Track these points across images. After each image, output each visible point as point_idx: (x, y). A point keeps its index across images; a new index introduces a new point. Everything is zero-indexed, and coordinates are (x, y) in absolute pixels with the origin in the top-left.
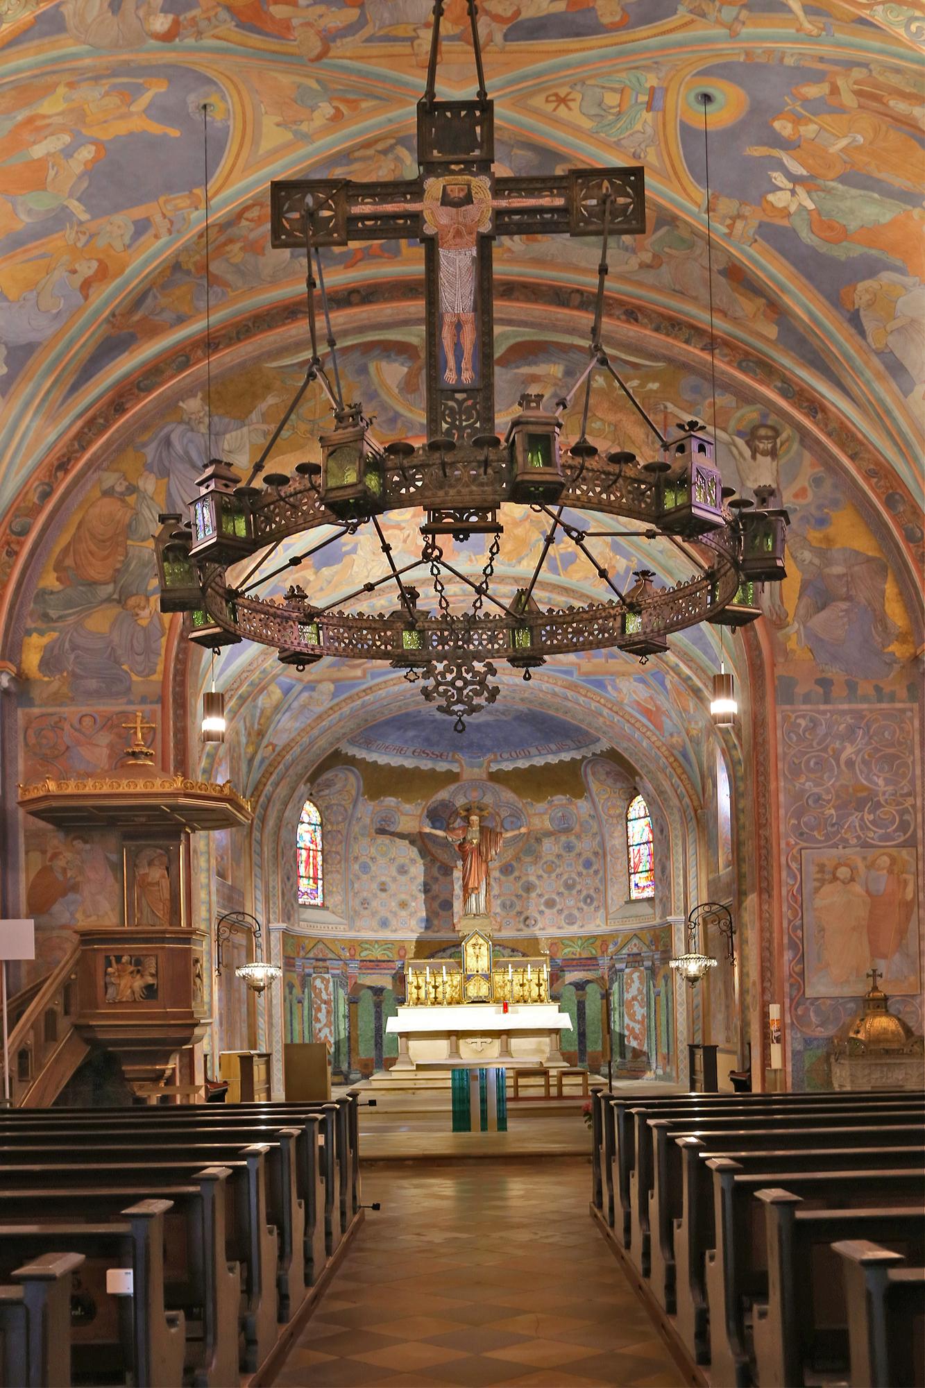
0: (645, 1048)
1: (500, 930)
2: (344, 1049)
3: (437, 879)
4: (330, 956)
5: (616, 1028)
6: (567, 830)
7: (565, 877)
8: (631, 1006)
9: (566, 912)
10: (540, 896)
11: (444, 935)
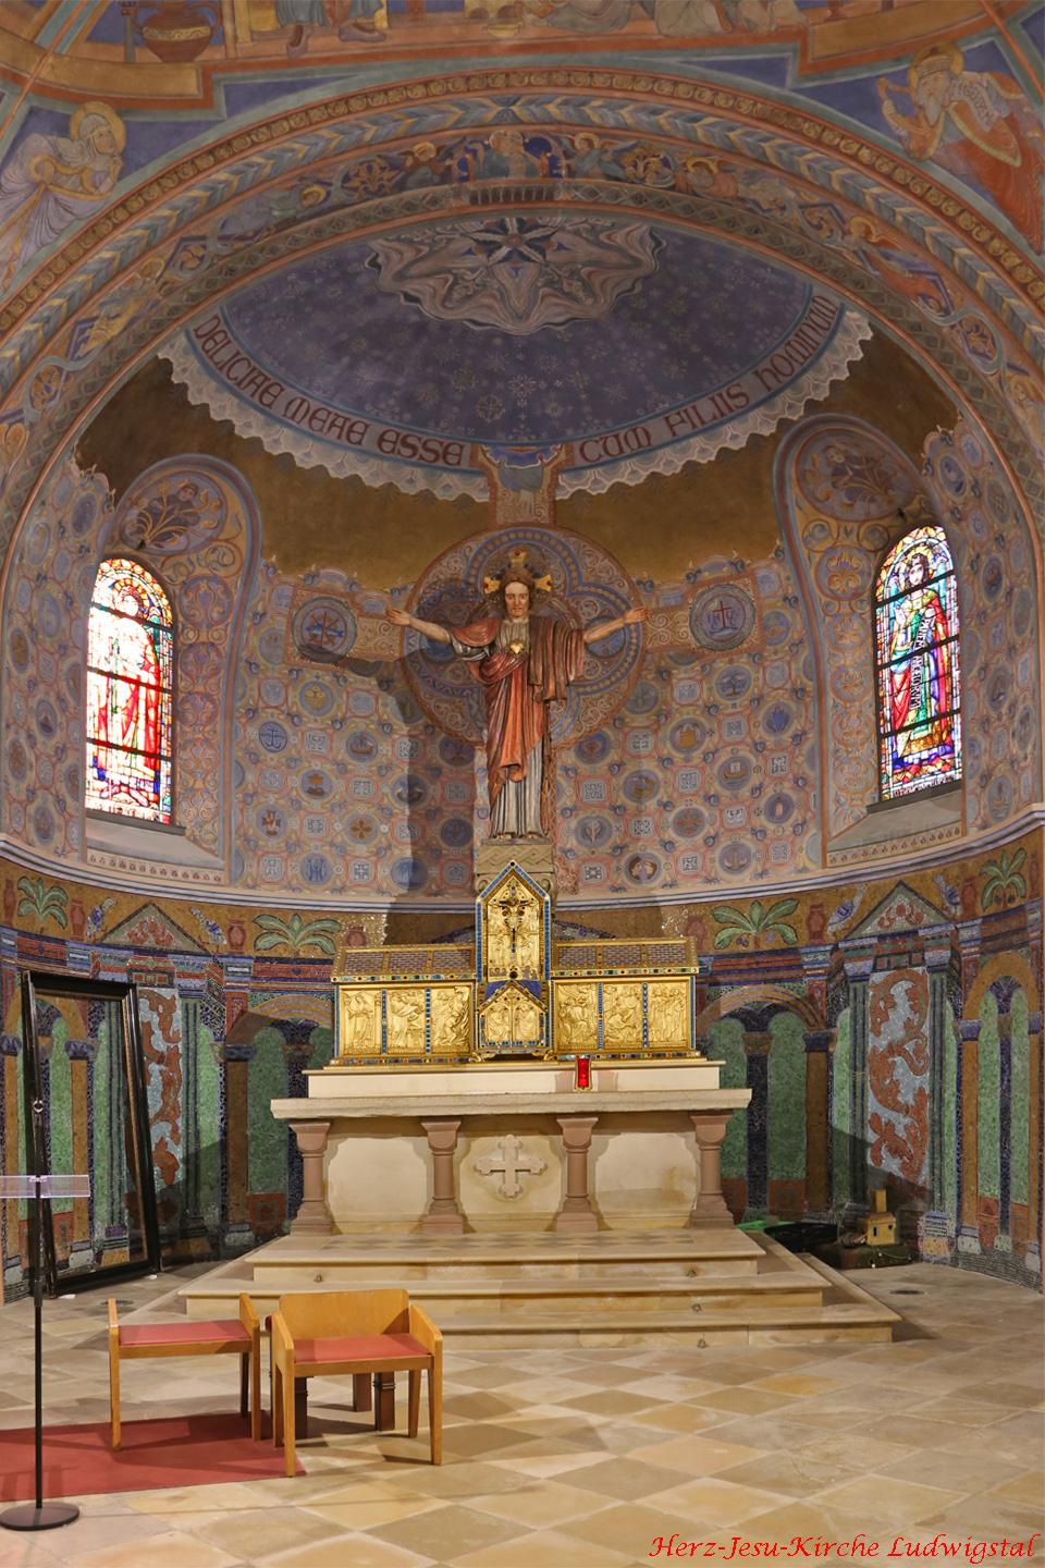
0: (924, 1177)
1: (574, 891)
2: (210, 1172)
3: (436, 772)
4: (178, 943)
5: (842, 1121)
6: (728, 646)
7: (724, 757)
8: (883, 1064)
9: (725, 842)
10: (666, 806)
11: (450, 901)
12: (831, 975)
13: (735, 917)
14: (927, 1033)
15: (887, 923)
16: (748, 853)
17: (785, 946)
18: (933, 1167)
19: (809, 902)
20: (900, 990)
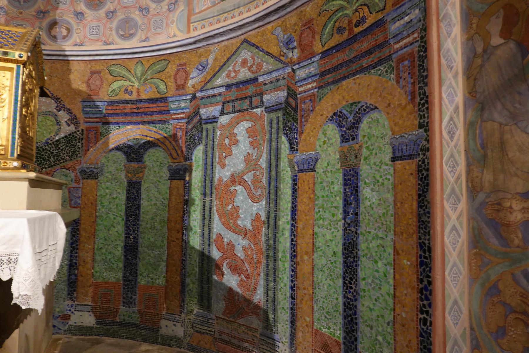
9: (120, 16)
12: (190, 119)
13: (124, 72)
14: (264, 166)
15: (233, 75)
16: (136, 24)
17: (158, 96)
18: (267, 288)
19: (177, 62)
20: (242, 129)
